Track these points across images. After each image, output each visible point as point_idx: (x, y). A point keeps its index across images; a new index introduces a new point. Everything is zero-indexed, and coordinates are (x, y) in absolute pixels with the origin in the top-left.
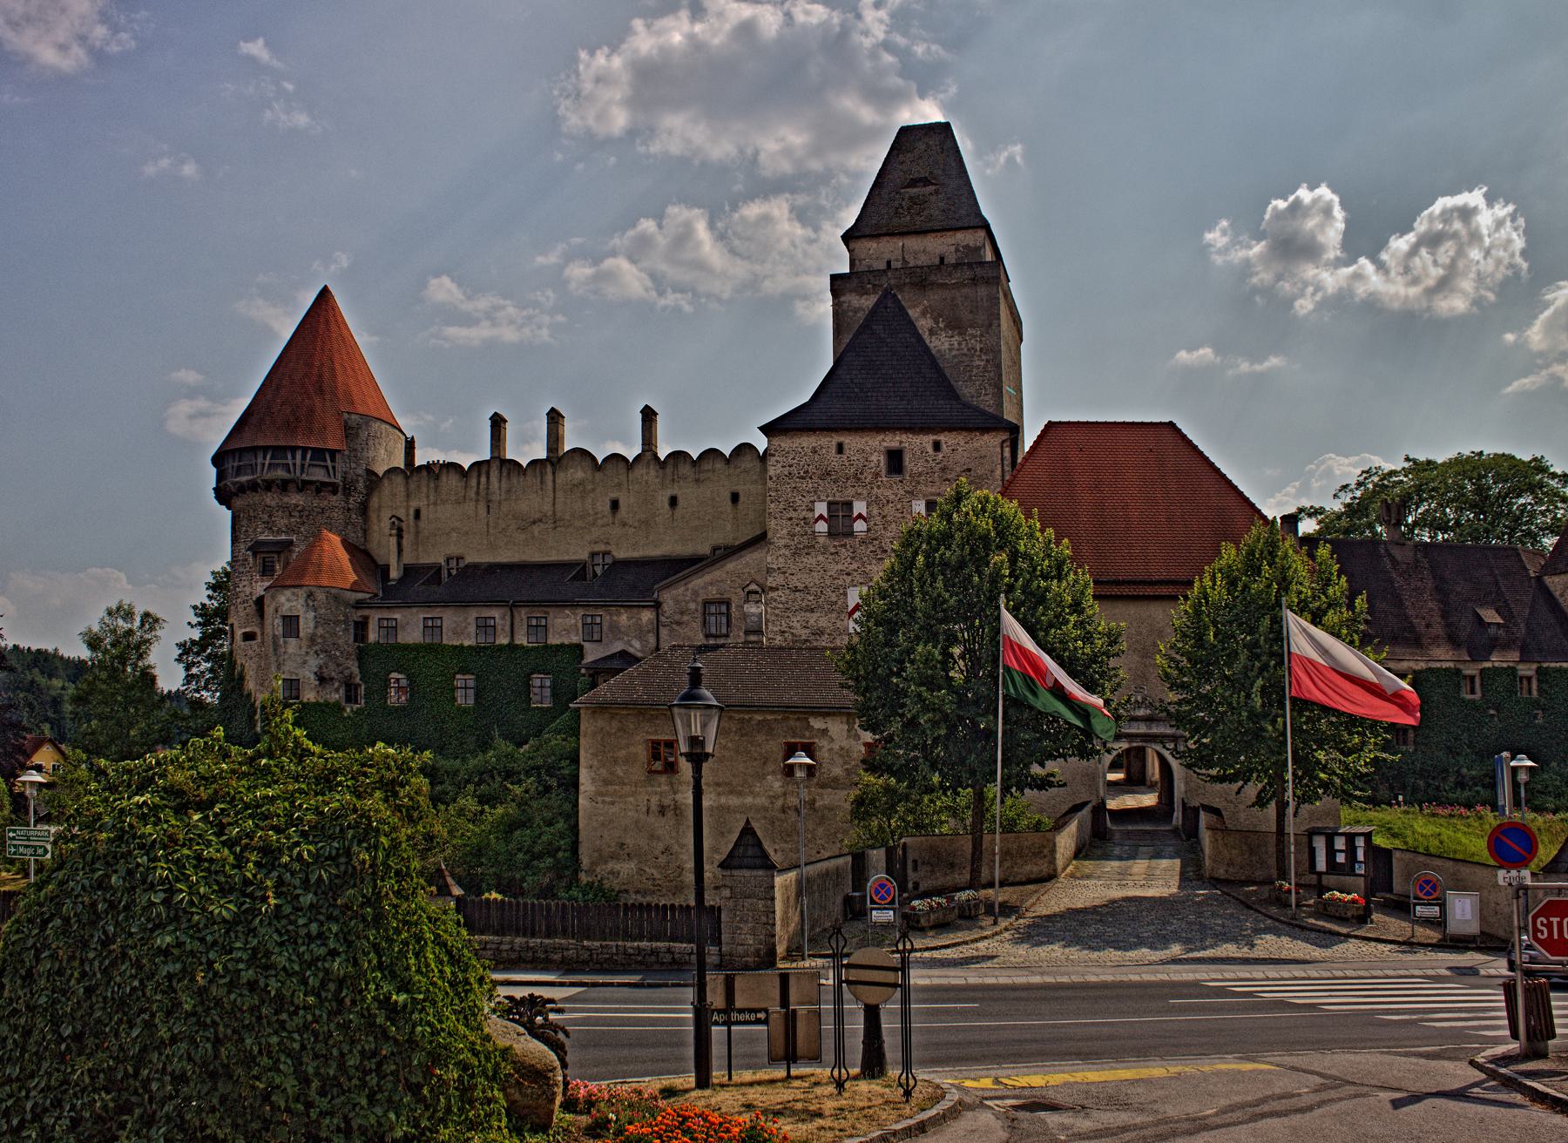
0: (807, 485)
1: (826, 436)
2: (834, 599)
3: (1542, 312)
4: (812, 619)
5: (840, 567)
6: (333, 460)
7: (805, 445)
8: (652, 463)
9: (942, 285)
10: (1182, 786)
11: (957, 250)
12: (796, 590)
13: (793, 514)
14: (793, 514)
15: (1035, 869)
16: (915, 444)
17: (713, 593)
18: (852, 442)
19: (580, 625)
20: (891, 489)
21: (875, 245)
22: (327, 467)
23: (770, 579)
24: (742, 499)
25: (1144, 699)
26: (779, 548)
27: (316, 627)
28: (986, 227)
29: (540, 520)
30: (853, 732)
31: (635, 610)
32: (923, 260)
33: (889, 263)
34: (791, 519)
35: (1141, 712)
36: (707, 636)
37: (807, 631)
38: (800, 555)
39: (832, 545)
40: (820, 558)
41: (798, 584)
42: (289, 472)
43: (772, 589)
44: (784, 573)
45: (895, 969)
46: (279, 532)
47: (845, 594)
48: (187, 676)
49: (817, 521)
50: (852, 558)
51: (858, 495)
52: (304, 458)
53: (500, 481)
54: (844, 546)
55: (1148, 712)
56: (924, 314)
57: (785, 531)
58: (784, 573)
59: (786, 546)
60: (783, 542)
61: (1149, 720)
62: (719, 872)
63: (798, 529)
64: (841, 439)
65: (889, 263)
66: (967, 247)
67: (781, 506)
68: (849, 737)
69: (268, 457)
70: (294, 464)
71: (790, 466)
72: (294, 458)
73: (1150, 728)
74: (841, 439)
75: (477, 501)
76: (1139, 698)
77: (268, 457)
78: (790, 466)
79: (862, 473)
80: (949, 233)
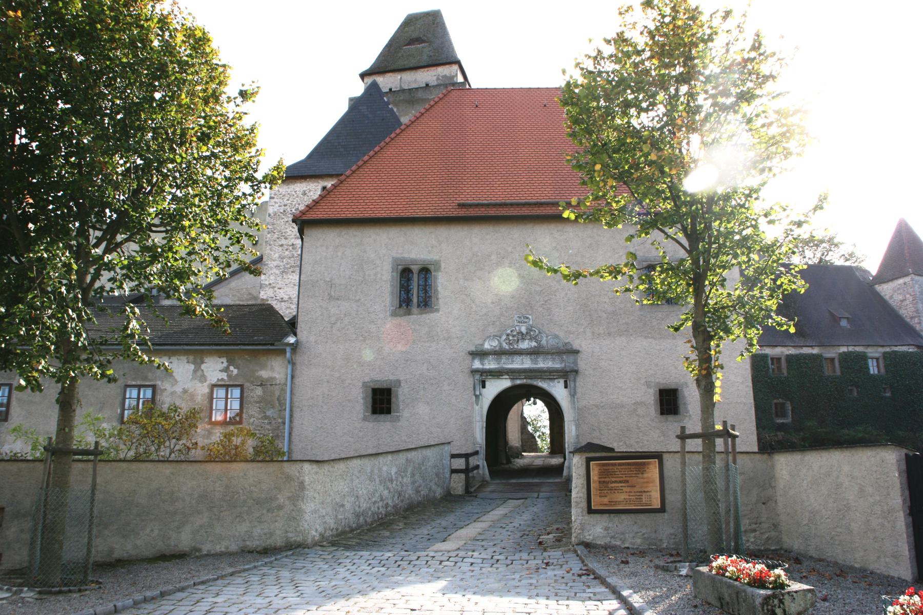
1: (314, 182)
7: (297, 189)
10: (574, 428)
11: (438, 79)
13: (283, 242)
14: (283, 242)
23: (262, 293)
25: (529, 330)
26: (271, 268)
28: (458, 63)
30: (199, 373)
34: (282, 245)
35: (525, 345)
38: (287, 273)
44: (274, 287)
55: (534, 344)
57: (277, 255)
58: (274, 287)
59: (277, 266)
60: (275, 263)
61: (534, 353)
63: (287, 253)
66: (445, 76)
67: (276, 236)
68: (194, 378)
71: (285, 205)
73: (536, 362)
76: (524, 330)
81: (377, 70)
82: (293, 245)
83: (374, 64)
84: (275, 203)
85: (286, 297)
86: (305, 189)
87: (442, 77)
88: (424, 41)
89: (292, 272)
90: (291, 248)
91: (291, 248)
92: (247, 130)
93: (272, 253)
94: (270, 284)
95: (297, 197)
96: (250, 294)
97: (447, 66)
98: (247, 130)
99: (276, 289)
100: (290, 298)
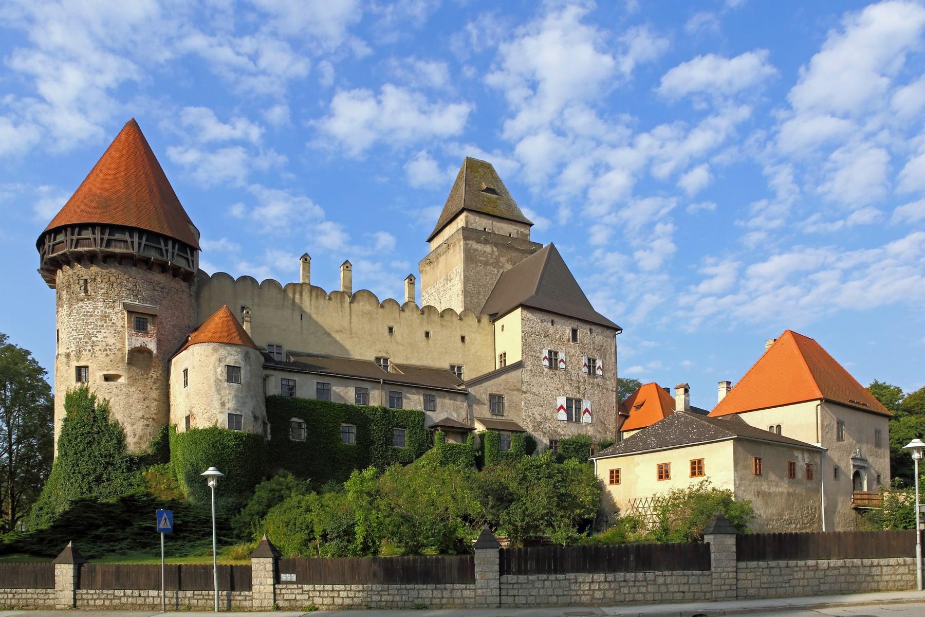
6: (192, 255)
8: (415, 310)
9: (516, 248)
11: (517, 233)
13: (533, 353)
14: (533, 353)
15: (44, 564)
17: (495, 391)
20: (574, 349)
21: (478, 218)
22: (187, 259)
27: (251, 378)
29: (341, 331)
32: (502, 233)
39: (551, 372)
42: (162, 255)
45: (622, 587)
53: (311, 300)
56: (508, 261)
62: (899, 525)
64: (553, 319)
65: (485, 229)
69: (144, 239)
70: (167, 251)
71: (532, 328)
72: (166, 245)
75: (293, 310)
77: (144, 239)
78: (532, 328)
85: (537, 393)
96: (515, 386)
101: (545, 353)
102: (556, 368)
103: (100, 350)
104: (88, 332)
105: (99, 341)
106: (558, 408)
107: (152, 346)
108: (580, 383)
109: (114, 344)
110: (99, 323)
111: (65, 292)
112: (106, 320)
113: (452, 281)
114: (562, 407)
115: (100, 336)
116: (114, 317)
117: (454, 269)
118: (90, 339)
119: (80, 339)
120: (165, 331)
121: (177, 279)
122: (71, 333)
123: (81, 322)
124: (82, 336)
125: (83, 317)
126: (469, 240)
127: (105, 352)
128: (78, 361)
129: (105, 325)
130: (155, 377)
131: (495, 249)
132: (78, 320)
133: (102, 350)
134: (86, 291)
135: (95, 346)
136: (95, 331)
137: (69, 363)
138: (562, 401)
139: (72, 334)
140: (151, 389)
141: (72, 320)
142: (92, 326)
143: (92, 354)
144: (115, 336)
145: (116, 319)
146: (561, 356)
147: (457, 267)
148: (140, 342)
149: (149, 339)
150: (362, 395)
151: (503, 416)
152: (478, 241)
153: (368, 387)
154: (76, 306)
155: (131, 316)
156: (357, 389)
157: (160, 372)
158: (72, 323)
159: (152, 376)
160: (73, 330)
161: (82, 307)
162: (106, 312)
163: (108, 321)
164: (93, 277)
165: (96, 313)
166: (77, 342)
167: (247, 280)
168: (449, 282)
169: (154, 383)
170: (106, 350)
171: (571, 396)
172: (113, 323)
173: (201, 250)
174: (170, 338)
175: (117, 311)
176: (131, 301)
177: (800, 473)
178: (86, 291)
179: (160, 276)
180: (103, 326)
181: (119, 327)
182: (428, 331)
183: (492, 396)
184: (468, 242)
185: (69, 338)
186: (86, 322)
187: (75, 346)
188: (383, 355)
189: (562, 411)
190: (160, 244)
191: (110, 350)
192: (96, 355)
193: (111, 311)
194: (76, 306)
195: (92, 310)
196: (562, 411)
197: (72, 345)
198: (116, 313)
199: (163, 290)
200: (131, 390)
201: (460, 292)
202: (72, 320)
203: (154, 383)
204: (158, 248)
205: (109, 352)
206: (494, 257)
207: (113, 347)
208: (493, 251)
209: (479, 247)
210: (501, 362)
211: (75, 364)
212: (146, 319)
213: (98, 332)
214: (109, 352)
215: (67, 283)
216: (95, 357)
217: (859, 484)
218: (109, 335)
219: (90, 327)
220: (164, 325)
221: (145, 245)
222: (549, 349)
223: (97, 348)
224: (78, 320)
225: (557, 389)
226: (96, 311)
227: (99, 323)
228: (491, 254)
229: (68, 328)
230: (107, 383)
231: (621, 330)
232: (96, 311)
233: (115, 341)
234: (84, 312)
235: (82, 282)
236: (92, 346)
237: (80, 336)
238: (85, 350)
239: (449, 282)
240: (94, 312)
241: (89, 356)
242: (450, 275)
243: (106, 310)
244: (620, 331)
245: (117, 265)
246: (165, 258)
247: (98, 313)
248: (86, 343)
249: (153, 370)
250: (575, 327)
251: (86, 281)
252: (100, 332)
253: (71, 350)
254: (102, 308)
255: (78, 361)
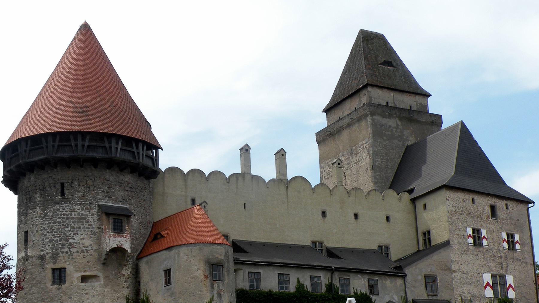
0: (462, 218)
2: (478, 279)
3: (447, 182)
4: (471, 288)
5: (479, 262)
7: (460, 197)
11: (417, 105)
12: (463, 273)
13: (458, 232)
14: (458, 232)
16: (500, 204)
17: (428, 271)
18: (479, 199)
19: (367, 284)
24: (391, 220)
31: (393, 278)
33: (387, 103)
34: (458, 235)
36: (428, 295)
37: (470, 295)
40: (471, 257)
41: (464, 270)
43: (454, 271)
44: (458, 263)
46: (117, 200)
47: (482, 277)
48: (513, 250)
49: (468, 237)
50: (484, 258)
51: (482, 226)
52: (54, 141)
54: (479, 251)
58: (458, 263)
65: (387, 103)
70: (138, 153)
71: (455, 207)
72: (76, 140)
74: (474, 197)
77: (120, 143)
79: (482, 216)
80: (413, 95)
81: (336, 102)
82: (463, 235)
83: (334, 94)
84: (450, 204)
85: (465, 272)
86: (464, 198)
87: (419, 103)
88: (392, 66)
89: (466, 254)
90: (462, 237)
91: (462, 237)
92: (58, 183)
93: (454, 239)
94: (456, 261)
95: (460, 202)
96: (446, 266)
97: (422, 97)
98: (58, 183)
99: (459, 264)
100: (467, 271)
101: (470, 231)
102: (481, 245)
103: (77, 252)
104: (65, 234)
105: (76, 243)
106: (485, 284)
107: (127, 246)
108: (503, 259)
109: (91, 245)
110: (76, 225)
111: (38, 195)
112: (82, 222)
113: (358, 155)
114: (488, 284)
115: (77, 238)
116: (90, 219)
117: (360, 144)
118: (67, 240)
119: (56, 241)
120: (134, 230)
121: (141, 177)
122: (45, 235)
123: (57, 224)
124: (58, 239)
125: (60, 220)
126: (375, 115)
127: (82, 254)
128: (54, 263)
129: (82, 227)
130: (126, 275)
131: (399, 123)
132: (53, 223)
133: (80, 251)
134: (63, 194)
135: (73, 247)
136: (72, 233)
137: (43, 265)
138: (487, 278)
139: (47, 236)
140: (123, 287)
141: (47, 223)
142: (69, 229)
143: (69, 256)
144: (91, 237)
145: (92, 221)
146: (484, 233)
147: (364, 142)
148: (117, 242)
149: (125, 239)
150: (283, 280)
151: (437, 295)
152: (384, 116)
153: (321, 275)
154: (52, 209)
155: (109, 218)
156: (312, 278)
157: (130, 270)
158: (47, 225)
159: (124, 275)
160: (48, 232)
161: (58, 210)
162: (82, 214)
163: (85, 223)
164: (70, 181)
165: (73, 216)
166: (53, 245)
167: (196, 172)
168: (354, 156)
169: (126, 281)
170: (83, 251)
171: (495, 273)
172: (90, 225)
173: (162, 149)
174: (137, 236)
175: (93, 212)
176: (106, 202)
177: (91, 236)
178: (63, 194)
179: (129, 176)
180: (80, 228)
181: (95, 229)
182: (356, 212)
183: (426, 277)
184: (374, 117)
185: (43, 240)
186: (63, 225)
187: (51, 248)
188: (317, 239)
189: (488, 287)
190: (133, 148)
191: (87, 252)
192: (74, 257)
193: (87, 213)
194: (52, 209)
195: (68, 212)
196: (488, 287)
197: (47, 247)
198: (93, 215)
199: (131, 190)
200: (106, 290)
201: (369, 168)
202: (47, 223)
203: (126, 281)
204: (131, 151)
205: (86, 254)
206: (399, 130)
207: (90, 248)
208: (397, 125)
209: (385, 121)
210: (425, 240)
211: (50, 266)
212: (121, 220)
213: (74, 234)
214: (86, 254)
215: (41, 187)
216: (72, 258)
217: (289, 284)
218: (86, 236)
219: (66, 229)
220: (133, 224)
221: (121, 149)
222: (472, 227)
223: (74, 250)
224: (53, 223)
225: (483, 267)
226: (73, 213)
227: (76, 225)
228: (396, 128)
229: (41, 230)
230: (83, 284)
231: (534, 203)
232: (73, 213)
233: (92, 243)
234: (61, 215)
235: (58, 186)
236: (69, 248)
237: (56, 238)
238: (63, 252)
239: (354, 156)
240: (71, 214)
241: (66, 259)
242: (356, 149)
243: (83, 212)
244: (532, 204)
245: (93, 168)
246: (137, 160)
247: (75, 215)
248: (63, 245)
249: (124, 269)
250: (493, 203)
251: (62, 185)
252: (77, 234)
253: (45, 252)
254: (79, 211)
255: (54, 263)
